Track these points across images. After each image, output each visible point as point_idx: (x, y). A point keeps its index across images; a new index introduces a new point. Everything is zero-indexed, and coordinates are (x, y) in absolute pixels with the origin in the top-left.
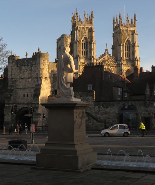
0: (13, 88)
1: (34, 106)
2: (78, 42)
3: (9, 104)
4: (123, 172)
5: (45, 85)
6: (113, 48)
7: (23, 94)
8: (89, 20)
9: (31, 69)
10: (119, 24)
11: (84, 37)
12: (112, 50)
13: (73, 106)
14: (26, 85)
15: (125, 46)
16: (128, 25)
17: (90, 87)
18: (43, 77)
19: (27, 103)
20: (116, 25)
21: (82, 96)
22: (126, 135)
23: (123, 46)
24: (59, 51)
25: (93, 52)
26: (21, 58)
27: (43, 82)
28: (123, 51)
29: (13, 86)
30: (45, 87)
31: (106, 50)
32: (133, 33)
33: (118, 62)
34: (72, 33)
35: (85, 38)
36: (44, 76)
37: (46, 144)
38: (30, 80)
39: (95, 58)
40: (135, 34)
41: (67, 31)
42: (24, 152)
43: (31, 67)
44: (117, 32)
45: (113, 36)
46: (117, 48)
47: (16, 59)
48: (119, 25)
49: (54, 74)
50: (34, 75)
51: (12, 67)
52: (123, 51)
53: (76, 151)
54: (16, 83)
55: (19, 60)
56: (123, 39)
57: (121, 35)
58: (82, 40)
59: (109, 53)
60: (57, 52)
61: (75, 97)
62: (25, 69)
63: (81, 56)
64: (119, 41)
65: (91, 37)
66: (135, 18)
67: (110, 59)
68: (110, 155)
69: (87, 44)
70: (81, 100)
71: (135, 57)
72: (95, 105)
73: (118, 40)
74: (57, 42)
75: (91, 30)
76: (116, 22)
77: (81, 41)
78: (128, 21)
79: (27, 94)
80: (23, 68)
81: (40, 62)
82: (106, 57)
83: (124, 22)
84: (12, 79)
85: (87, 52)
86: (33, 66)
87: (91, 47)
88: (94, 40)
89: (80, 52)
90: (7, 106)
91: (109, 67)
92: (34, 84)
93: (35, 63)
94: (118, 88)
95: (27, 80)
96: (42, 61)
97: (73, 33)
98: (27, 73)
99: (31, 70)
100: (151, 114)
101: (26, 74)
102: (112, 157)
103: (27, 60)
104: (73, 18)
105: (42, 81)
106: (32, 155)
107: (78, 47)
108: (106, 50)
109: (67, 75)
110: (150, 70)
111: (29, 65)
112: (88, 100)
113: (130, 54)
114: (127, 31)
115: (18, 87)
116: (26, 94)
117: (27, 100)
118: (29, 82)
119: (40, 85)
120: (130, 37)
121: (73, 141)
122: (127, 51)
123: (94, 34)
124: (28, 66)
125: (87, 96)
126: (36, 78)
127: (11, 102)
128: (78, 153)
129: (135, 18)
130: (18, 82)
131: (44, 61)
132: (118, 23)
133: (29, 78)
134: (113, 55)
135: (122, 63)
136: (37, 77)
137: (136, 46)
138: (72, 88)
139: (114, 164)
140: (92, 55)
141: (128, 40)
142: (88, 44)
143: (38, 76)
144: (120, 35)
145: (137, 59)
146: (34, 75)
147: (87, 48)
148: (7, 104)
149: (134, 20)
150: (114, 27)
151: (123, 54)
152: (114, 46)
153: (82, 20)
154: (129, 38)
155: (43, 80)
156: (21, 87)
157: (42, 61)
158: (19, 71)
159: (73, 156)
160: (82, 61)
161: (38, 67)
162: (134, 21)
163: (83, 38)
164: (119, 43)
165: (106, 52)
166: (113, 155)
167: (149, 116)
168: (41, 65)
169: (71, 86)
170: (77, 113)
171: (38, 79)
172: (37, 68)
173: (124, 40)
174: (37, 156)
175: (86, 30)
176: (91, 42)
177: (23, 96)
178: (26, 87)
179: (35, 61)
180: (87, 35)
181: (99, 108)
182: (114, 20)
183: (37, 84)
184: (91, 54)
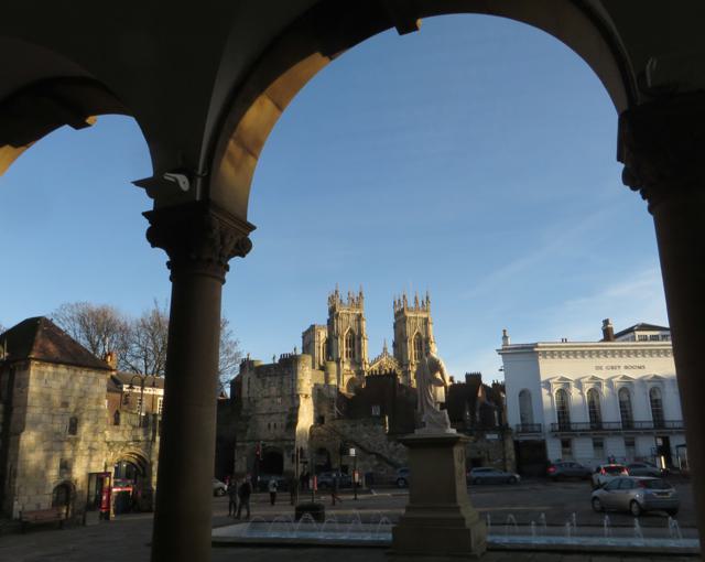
3: (244, 441)
4: (266, 550)
6: (395, 345)
8: (357, 302)
13: (452, 442)
16: (416, 310)
17: (376, 411)
23: (342, 339)
26: (263, 363)
29: (250, 410)
31: (385, 349)
32: (426, 321)
34: (330, 323)
35: (351, 331)
36: (305, 392)
37: (408, 509)
38: (279, 400)
41: (322, 318)
42: (324, 525)
44: (400, 320)
45: (395, 327)
47: (256, 364)
49: (319, 390)
50: (287, 391)
53: (463, 519)
55: (262, 366)
57: (407, 324)
61: (452, 427)
63: (345, 359)
65: (360, 329)
66: (427, 298)
68: (513, 524)
70: (458, 431)
72: (389, 440)
74: (303, 337)
75: (359, 318)
78: (416, 302)
81: (296, 370)
82: (384, 360)
83: (411, 304)
88: (365, 332)
98: (274, 388)
99: (282, 383)
100: (482, 453)
101: (274, 390)
102: (517, 528)
103: (273, 365)
104: (331, 299)
106: (385, 531)
108: (385, 349)
109: (436, 392)
110: (463, 380)
114: (416, 318)
116: (272, 424)
119: (297, 407)
121: (455, 501)
123: (364, 324)
127: (247, 438)
128: (467, 523)
129: (427, 298)
136: (293, 394)
138: (446, 411)
141: (418, 333)
142: (355, 341)
146: (287, 391)
153: (345, 301)
155: (302, 399)
156: (264, 412)
157: (300, 368)
158: (260, 385)
159: (460, 530)
160: (347, 367)
166: (519, 525)
167: (478, 456)
169: (442, 409)
170: (457, 450)
171: (294, 398)
174: (394, 531)
175: (352, 318)
176: (360, 336)
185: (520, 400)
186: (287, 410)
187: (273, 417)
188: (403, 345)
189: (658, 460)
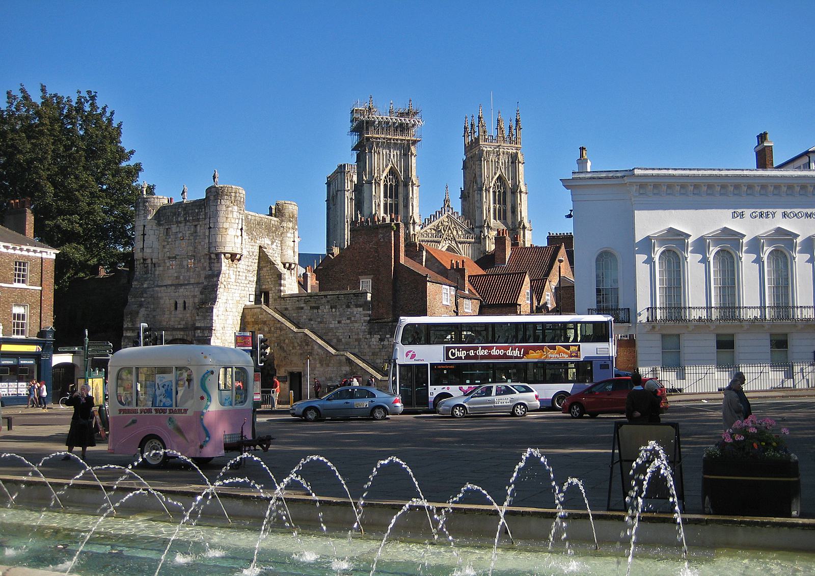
0: (145, 286)
1: (200, 335)
2: (373, 181)
5: (233, 277)
6: (464, 196)
7: (172, 302)
9: (196, 232)
10: (479, 136)
11: (389, 167)
12: (463, 202)
14: (181, 278)
15: (494, 192)
18: (225, 254)
19: (182, 326)
20: (472, 140)
21: (335, 307)
22: (311, 415)
23: (487, 190)
24: (331, 206)
25: (413, 206)
27: (224, 268)
28: (489, 202)
30: (233, 280)
31: (446, 201)
32: (514, 159)
33: (477, 230)
35: (392, 172)
36: (229, 249)
39: (417, 220)
40: (519, 162)
43: (196, 226)
45: (465, 168)
46: (473, 196)
48: (477, 140)
51: (144, 226)
52: (489, 202)
54: (155, 270)
56: (488, 173)
58: (385, 174)
59: (452, 209)
60: (328, 209)
62: (180, 232)
64: (478, 179)
67: (455, 223)
69: (397, 186)
71: (519, 220)
73: (475, 177)
76: (471, 132)
77: (383, 178)
78: (499, 127)
79: (185, 302)
80: (174, 228)
84: (144, 260)
85: (397, 205)
86: (200, 223)
87: (408, 194)
89: (379, 205)
90: (128, 334)
91: (454, 244)
92: (202, 272)
93: (206, 214)
94: (444, 286)
95: (185, 263)
96: (224, 208)
97: (361, 158)
105: (223, 264)
107: (374, 193)
108: (446, 201)
111: (189, 221)
112: (353, 319)
113: (505, 211)
115: (160, 283)
117: (182, 319)
118: (188, 269)
120: (505, 169)
122: (499, 203)
124: (188, 223)
125: (348, 307)
126: (208, 257)
129: (517, 121)
130: (161, 268)
131: (230, 209)
132: (476, 135)
133: (190, 257)
134: (463, 214)
135: (486, 234)
137: (521, 192)
139: (243, 536)
140: (411, 214)
141: (500, 178)
143: (213, 249)
144: (481, 165)
145: (524, 225)
147: (397, 197)
148: (128, 329)
149: (516, 127)
150: (465, 145)
151: (489, 211)
152: (466, 191)
154: (503, 171)
161: (212, 225)
162: (516, 129)
163: (387, 170)
164: (479, 182)
165: (445, 205)
168: (221, 219)
172: (210, 228)
173: (489, 174)
177: (173, 308)
178: (182, 282)
179: (205, 208)
180: (397, 162)
181: (381, 340)
182: (465, 128)
183: (210, 272)
184: (408, 212)
185: (597, 268)
186: (202, 279)
187: (181, 290)
188: (477, 197)
189: (537, 334)
